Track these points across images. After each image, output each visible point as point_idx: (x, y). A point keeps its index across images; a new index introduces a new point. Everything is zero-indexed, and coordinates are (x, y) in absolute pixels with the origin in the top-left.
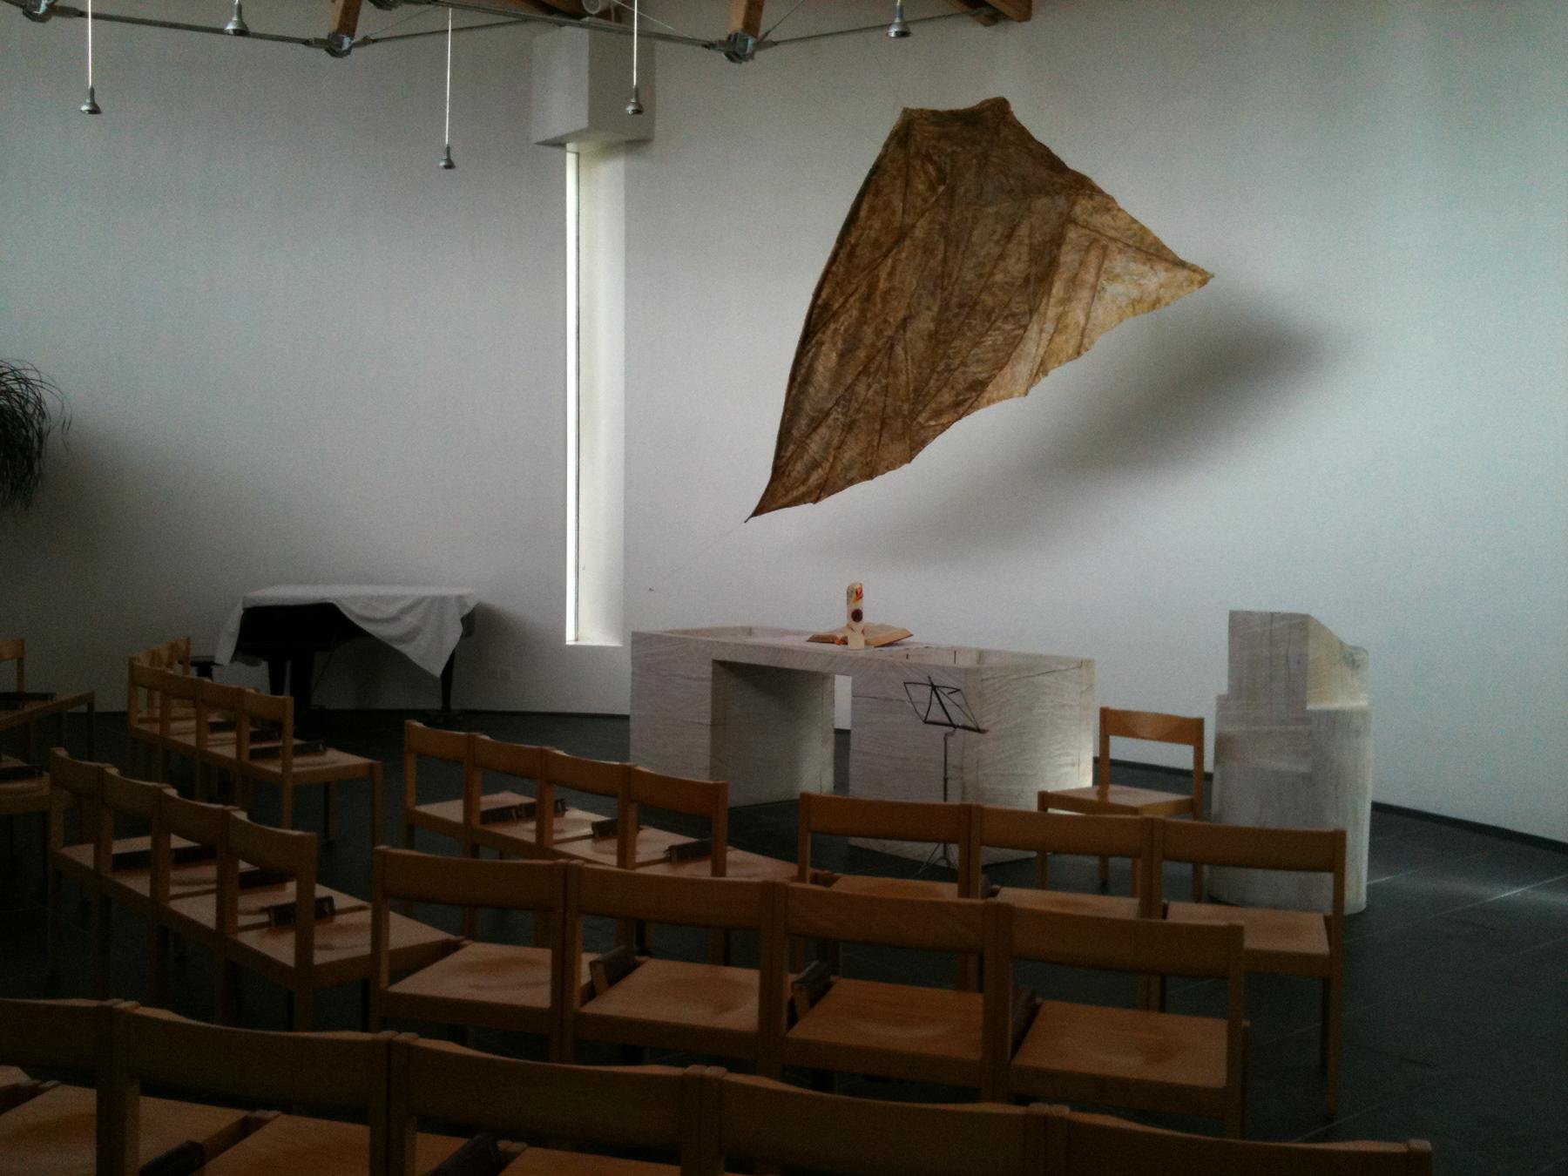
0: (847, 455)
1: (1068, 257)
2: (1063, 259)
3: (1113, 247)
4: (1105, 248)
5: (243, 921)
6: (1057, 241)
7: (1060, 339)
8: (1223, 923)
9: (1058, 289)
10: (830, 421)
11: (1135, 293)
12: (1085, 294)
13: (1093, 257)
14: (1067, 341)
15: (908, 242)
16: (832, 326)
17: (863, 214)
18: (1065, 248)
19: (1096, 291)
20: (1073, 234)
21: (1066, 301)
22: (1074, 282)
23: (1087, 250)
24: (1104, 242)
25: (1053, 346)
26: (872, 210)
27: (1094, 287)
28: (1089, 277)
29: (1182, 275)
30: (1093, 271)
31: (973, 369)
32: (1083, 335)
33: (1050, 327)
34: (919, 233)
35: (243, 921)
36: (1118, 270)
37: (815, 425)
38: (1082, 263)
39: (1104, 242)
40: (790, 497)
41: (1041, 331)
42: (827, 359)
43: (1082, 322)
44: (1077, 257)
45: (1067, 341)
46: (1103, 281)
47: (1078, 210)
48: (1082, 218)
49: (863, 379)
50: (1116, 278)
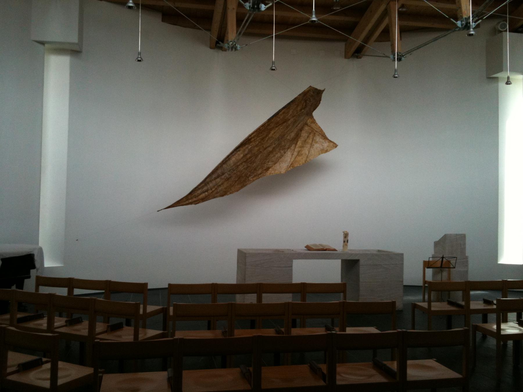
0: (220, 188)
1: (304, 134)
2: (302, 135)
3: (317, 134)
4: (315, 134)
5: (9, 370)
6: (301, 130)
7: (299, 158)
8: (390, 301)
9: (299, 143)
10: (223, 177)
11: (322, 147)
12: (308, 146)
13: (311, 136)
14: (302, 158)
15: (285, 124)
16: (247, 146)
17: (281, 113)
18: (303, 132)
19: (312, 145)
20: (306, 128)
21: (302, 147)
22: (305, 141)
23: (310, 133)
24: (315, 132)
25: (297, 159)
26: (283, 113)
27: (311, 144)
28: (310, 141)
29: (332, 144)
30: (311, 140)
31: (270, 163)
32: (307, 157)
33: (295, 154)
34: (289, 122)
35: (9, 370)
36: (317, 140)
37: (218, 177)
38: (308, 137)
39: (315, 132)
40: (187, 202)
41: (292, 155)
42: (240, 155)
43: (307, 153)
44: (307, 135)
45: (302, 158)
46: (313, 143)
47: (308, 121)
48: (309, 124)
49: (244, 164)
50: (317, 142)
